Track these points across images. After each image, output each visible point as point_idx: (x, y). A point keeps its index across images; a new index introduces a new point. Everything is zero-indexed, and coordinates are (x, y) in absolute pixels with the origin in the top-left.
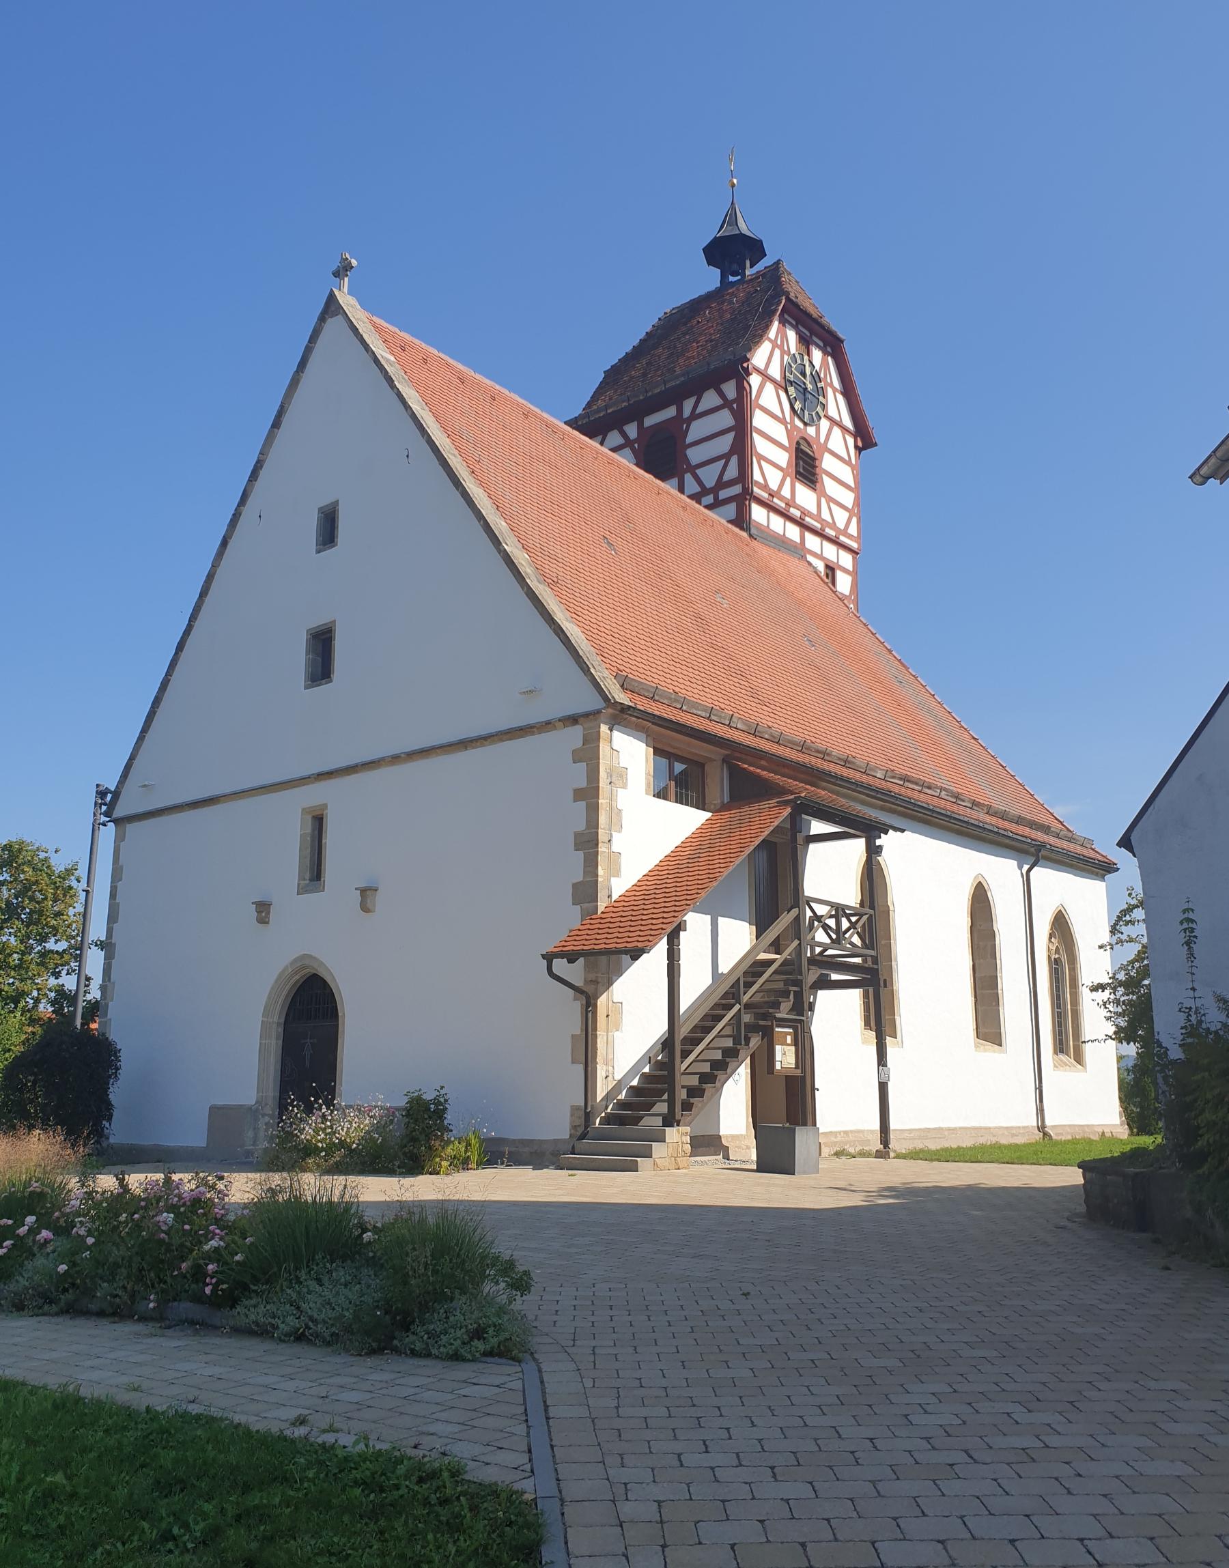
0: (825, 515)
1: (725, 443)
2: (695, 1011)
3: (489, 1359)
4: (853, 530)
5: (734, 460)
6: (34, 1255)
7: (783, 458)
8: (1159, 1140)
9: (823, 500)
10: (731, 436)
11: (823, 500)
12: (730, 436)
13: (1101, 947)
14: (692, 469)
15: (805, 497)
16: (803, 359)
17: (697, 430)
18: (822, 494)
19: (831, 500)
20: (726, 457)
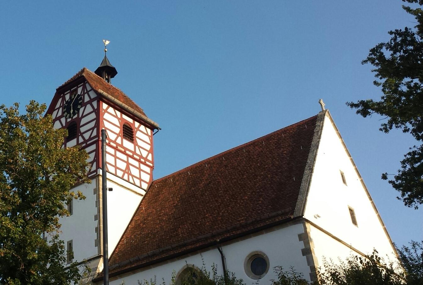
0: (138, 152)
1: (92, 124)
2: (316, 152)
3: (72, 212)
4: (150, 158)
5: (95, 129)
6: (389, 131)
7: (117, 130)
8: (380, 67)
9: (137, 147)
10: (94, 122)
11: (137, 147)
12: (94, 122)
13: (84, 198)
14: (82, 134)
15: (127, 144)
16: (195, 234)
17: (83, 121)
18: (136, 144)
19: (139, 147)
20: (93, 129)
